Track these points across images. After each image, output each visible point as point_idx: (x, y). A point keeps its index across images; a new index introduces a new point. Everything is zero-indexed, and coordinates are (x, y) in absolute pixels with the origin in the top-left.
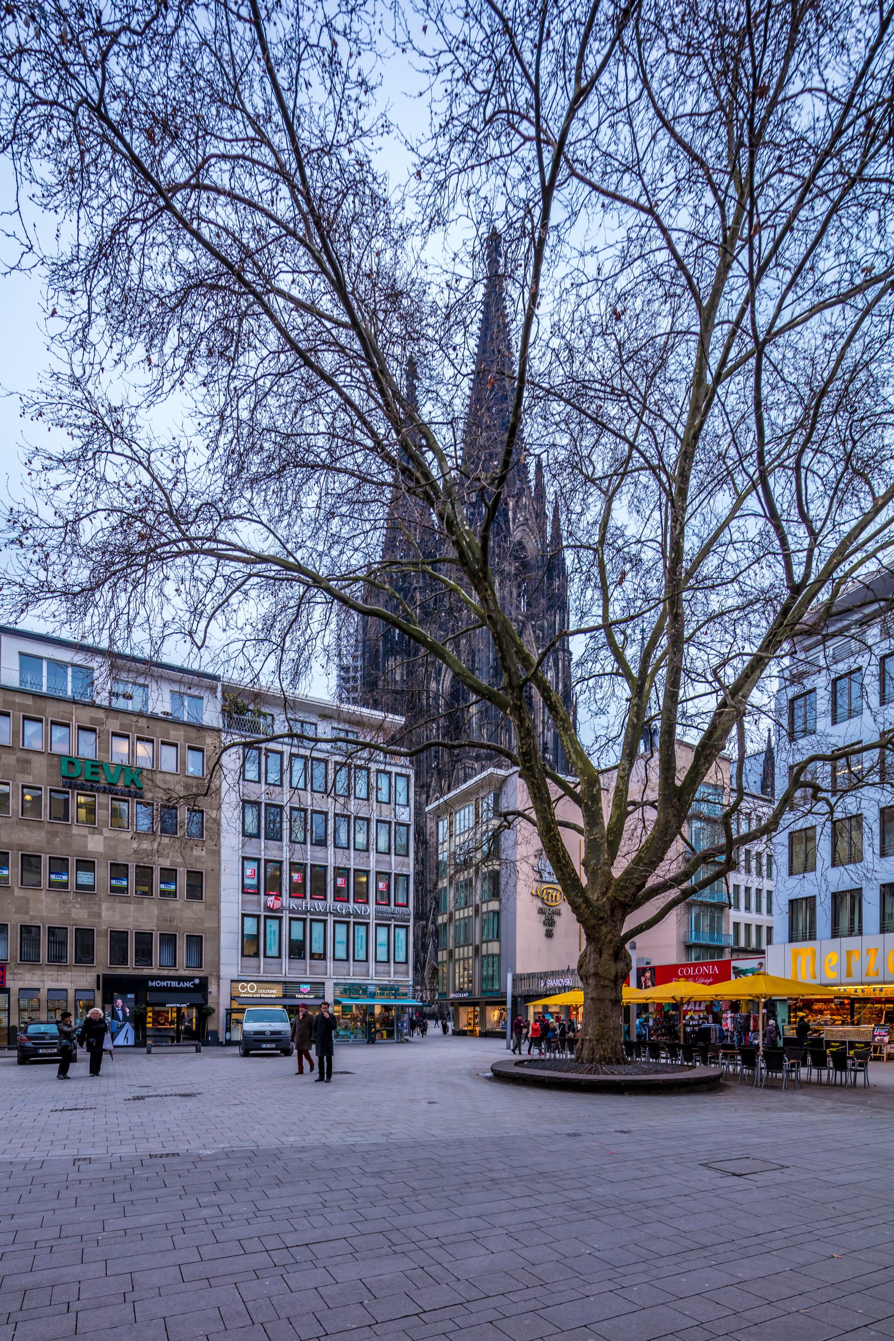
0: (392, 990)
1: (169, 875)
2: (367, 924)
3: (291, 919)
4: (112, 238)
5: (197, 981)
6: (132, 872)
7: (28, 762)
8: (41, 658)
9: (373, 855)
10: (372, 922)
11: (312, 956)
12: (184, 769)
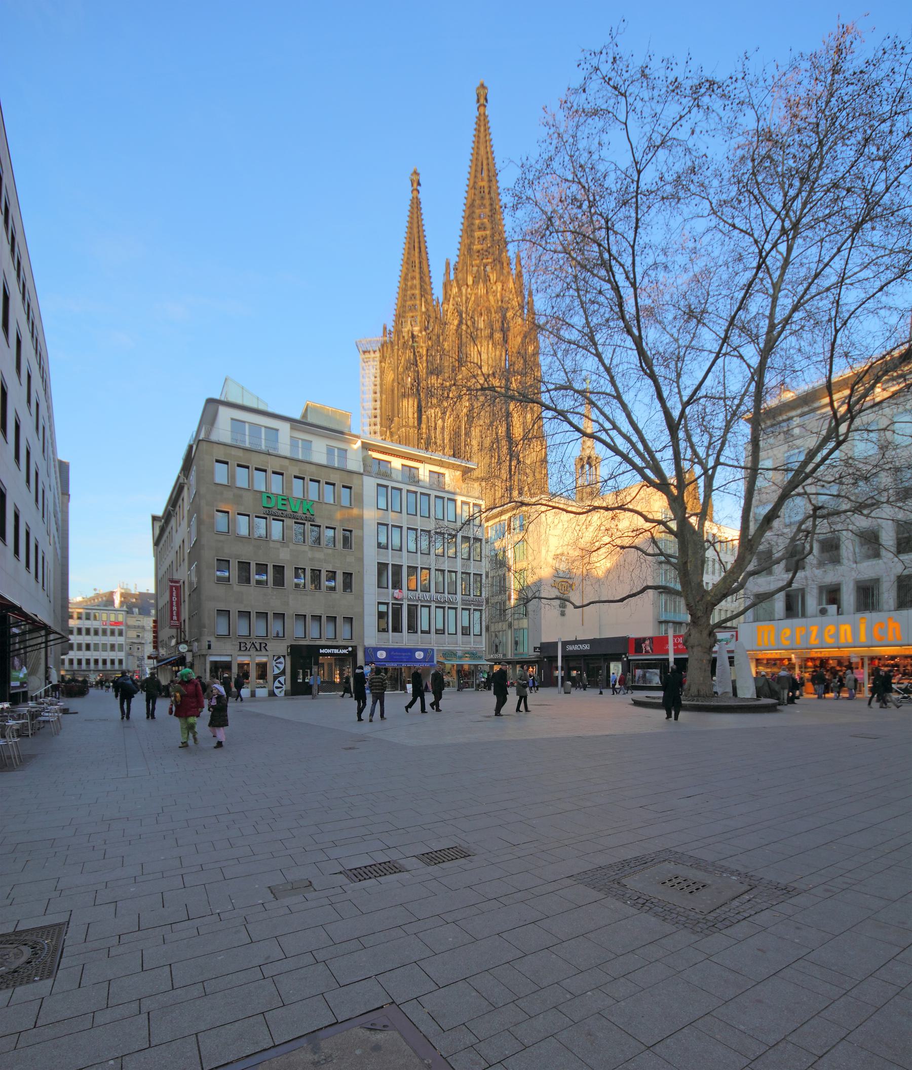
0: (473, 655)
1: (332, 575)
2: (456, 609)
3: (437, 607)
4: (708, 432)
5: (350, 649)
6: (270, 570)
7: (241, 496)
8: (244, 422)
9: (459, 560)
10: (460, 607)
11: (422, 632)
12: (340, 502)
